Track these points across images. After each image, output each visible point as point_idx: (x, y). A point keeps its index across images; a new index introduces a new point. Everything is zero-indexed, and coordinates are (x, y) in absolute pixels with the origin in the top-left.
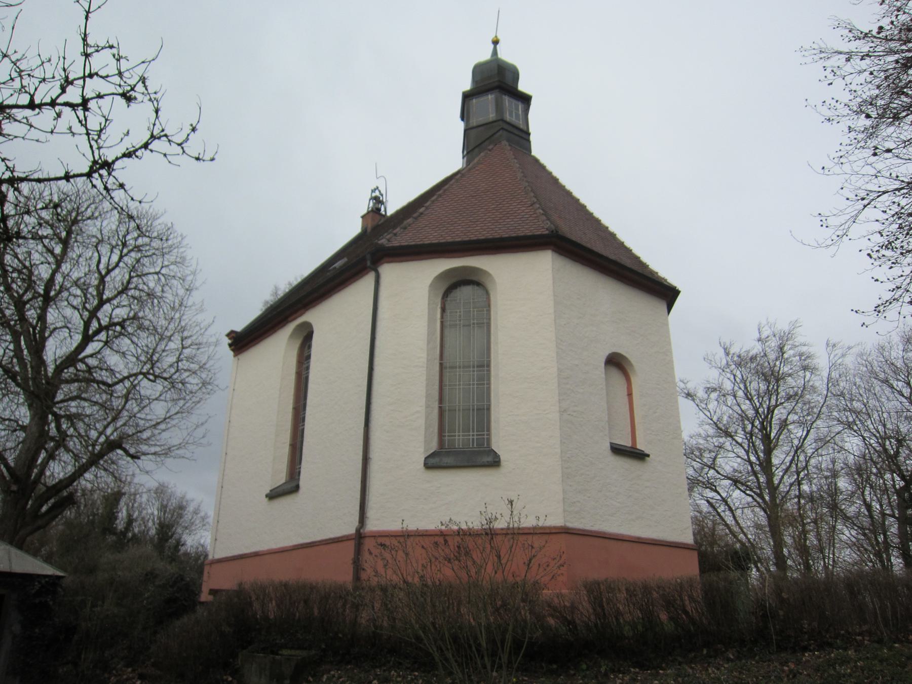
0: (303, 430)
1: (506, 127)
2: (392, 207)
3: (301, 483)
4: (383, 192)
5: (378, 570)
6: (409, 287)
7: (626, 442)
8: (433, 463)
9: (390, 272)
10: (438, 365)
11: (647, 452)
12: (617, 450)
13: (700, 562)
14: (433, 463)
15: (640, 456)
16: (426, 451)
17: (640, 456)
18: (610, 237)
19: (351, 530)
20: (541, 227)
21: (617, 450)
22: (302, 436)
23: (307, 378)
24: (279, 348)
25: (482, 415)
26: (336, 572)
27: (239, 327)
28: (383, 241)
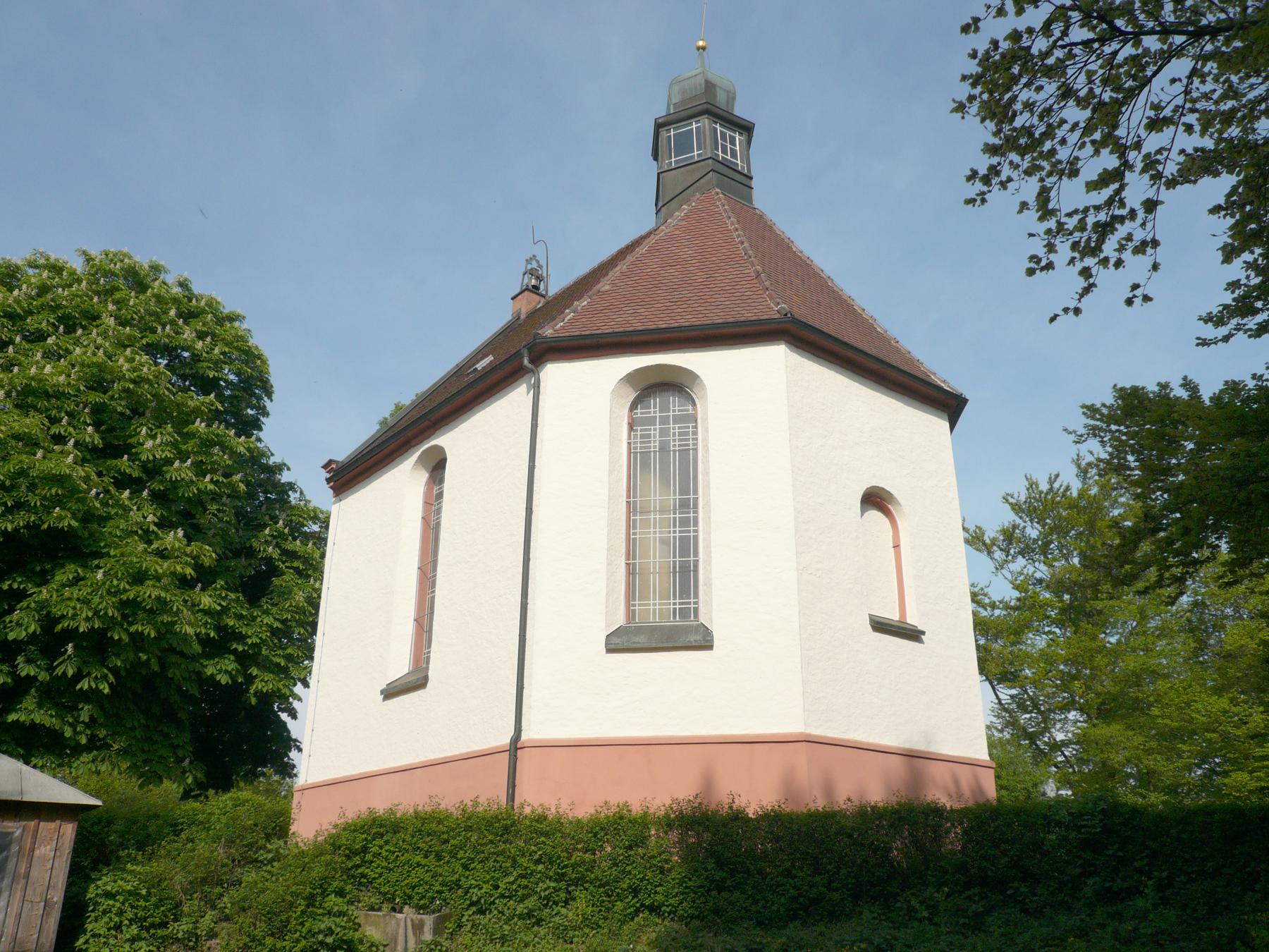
0: (433, 598)
1: (720, 168)
2: (555, 285)
3: (431, 674)
4: (543, 263)
5: (540, 794)
6: (583, 396)
7: (893, 615)
8: (619, 643)
9: (555, 374)
10: (624, 503)
11: (920, 628)
12: (880, 626)
13: (979, 659)
14: (619, 643)
15: (914, 635)
16: (608, 626)
17: (914, 635)
18: (865, 325)
19: (505, 739)
20: (771, 308)
21: (880, 626)
22: (432, 613)
23: (438, 525)
24: (402, 481)
25: (686, 577)
26: (487, 792)
27: (342, 454)
28: (548, 332)
